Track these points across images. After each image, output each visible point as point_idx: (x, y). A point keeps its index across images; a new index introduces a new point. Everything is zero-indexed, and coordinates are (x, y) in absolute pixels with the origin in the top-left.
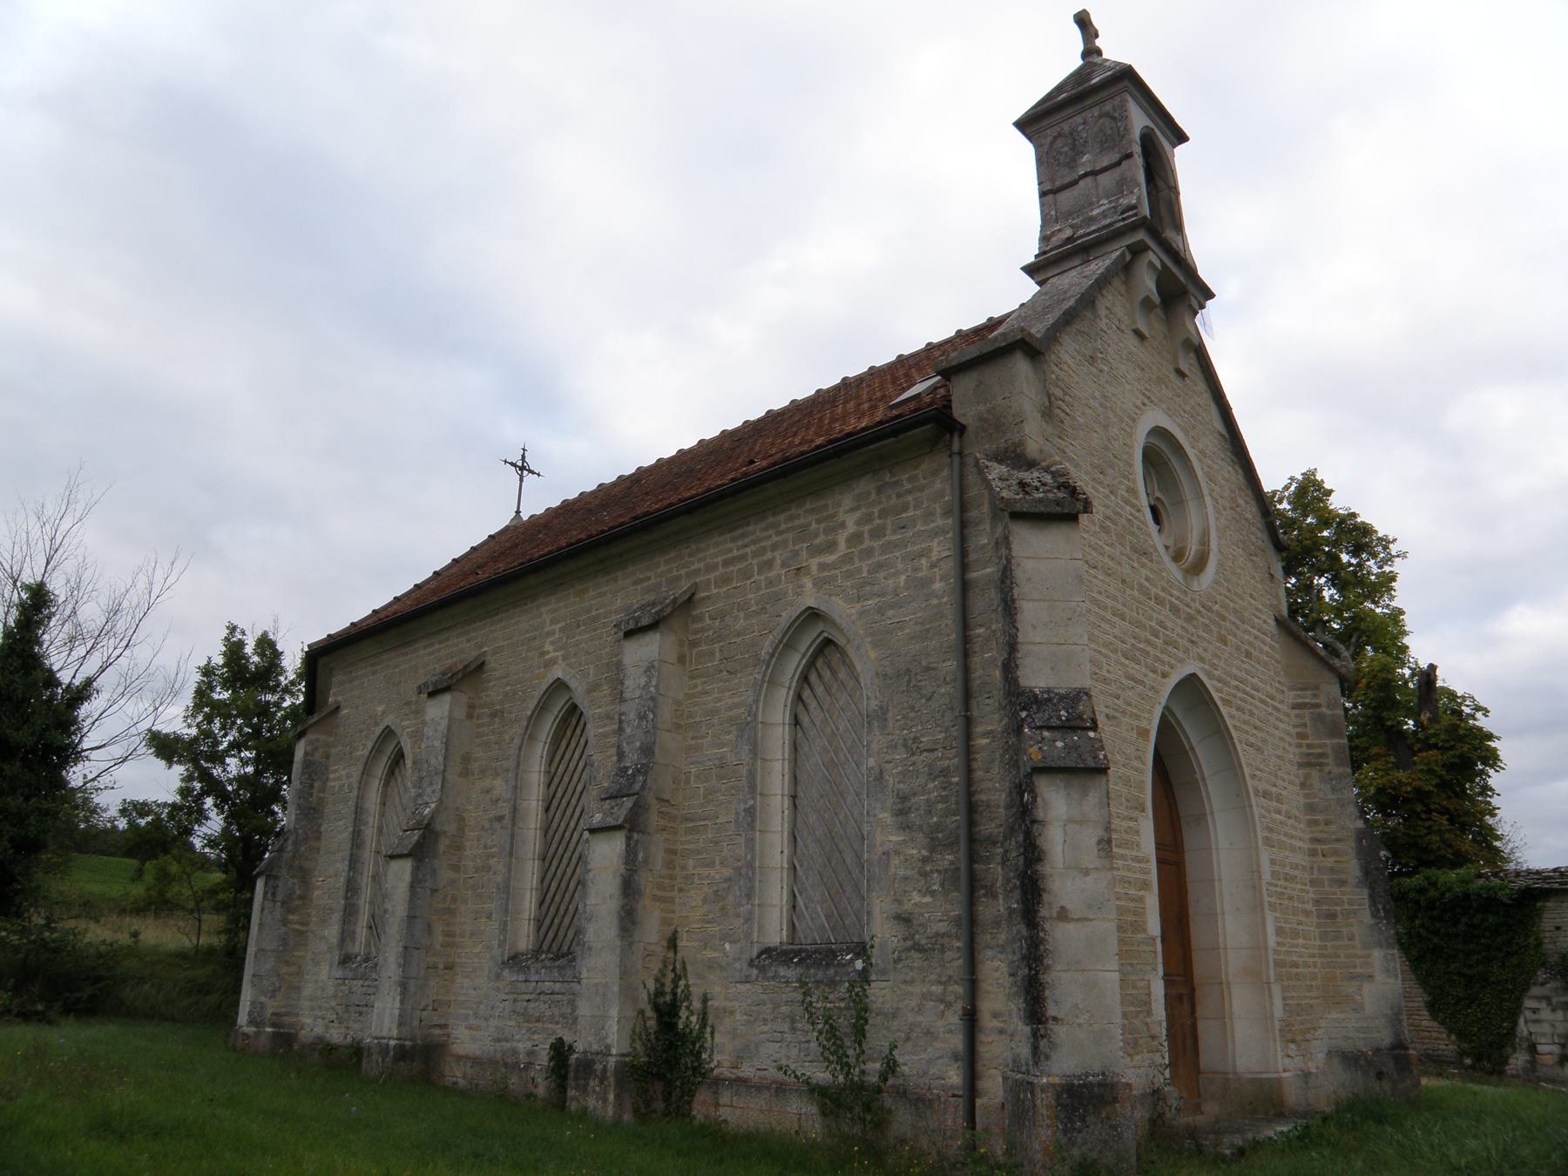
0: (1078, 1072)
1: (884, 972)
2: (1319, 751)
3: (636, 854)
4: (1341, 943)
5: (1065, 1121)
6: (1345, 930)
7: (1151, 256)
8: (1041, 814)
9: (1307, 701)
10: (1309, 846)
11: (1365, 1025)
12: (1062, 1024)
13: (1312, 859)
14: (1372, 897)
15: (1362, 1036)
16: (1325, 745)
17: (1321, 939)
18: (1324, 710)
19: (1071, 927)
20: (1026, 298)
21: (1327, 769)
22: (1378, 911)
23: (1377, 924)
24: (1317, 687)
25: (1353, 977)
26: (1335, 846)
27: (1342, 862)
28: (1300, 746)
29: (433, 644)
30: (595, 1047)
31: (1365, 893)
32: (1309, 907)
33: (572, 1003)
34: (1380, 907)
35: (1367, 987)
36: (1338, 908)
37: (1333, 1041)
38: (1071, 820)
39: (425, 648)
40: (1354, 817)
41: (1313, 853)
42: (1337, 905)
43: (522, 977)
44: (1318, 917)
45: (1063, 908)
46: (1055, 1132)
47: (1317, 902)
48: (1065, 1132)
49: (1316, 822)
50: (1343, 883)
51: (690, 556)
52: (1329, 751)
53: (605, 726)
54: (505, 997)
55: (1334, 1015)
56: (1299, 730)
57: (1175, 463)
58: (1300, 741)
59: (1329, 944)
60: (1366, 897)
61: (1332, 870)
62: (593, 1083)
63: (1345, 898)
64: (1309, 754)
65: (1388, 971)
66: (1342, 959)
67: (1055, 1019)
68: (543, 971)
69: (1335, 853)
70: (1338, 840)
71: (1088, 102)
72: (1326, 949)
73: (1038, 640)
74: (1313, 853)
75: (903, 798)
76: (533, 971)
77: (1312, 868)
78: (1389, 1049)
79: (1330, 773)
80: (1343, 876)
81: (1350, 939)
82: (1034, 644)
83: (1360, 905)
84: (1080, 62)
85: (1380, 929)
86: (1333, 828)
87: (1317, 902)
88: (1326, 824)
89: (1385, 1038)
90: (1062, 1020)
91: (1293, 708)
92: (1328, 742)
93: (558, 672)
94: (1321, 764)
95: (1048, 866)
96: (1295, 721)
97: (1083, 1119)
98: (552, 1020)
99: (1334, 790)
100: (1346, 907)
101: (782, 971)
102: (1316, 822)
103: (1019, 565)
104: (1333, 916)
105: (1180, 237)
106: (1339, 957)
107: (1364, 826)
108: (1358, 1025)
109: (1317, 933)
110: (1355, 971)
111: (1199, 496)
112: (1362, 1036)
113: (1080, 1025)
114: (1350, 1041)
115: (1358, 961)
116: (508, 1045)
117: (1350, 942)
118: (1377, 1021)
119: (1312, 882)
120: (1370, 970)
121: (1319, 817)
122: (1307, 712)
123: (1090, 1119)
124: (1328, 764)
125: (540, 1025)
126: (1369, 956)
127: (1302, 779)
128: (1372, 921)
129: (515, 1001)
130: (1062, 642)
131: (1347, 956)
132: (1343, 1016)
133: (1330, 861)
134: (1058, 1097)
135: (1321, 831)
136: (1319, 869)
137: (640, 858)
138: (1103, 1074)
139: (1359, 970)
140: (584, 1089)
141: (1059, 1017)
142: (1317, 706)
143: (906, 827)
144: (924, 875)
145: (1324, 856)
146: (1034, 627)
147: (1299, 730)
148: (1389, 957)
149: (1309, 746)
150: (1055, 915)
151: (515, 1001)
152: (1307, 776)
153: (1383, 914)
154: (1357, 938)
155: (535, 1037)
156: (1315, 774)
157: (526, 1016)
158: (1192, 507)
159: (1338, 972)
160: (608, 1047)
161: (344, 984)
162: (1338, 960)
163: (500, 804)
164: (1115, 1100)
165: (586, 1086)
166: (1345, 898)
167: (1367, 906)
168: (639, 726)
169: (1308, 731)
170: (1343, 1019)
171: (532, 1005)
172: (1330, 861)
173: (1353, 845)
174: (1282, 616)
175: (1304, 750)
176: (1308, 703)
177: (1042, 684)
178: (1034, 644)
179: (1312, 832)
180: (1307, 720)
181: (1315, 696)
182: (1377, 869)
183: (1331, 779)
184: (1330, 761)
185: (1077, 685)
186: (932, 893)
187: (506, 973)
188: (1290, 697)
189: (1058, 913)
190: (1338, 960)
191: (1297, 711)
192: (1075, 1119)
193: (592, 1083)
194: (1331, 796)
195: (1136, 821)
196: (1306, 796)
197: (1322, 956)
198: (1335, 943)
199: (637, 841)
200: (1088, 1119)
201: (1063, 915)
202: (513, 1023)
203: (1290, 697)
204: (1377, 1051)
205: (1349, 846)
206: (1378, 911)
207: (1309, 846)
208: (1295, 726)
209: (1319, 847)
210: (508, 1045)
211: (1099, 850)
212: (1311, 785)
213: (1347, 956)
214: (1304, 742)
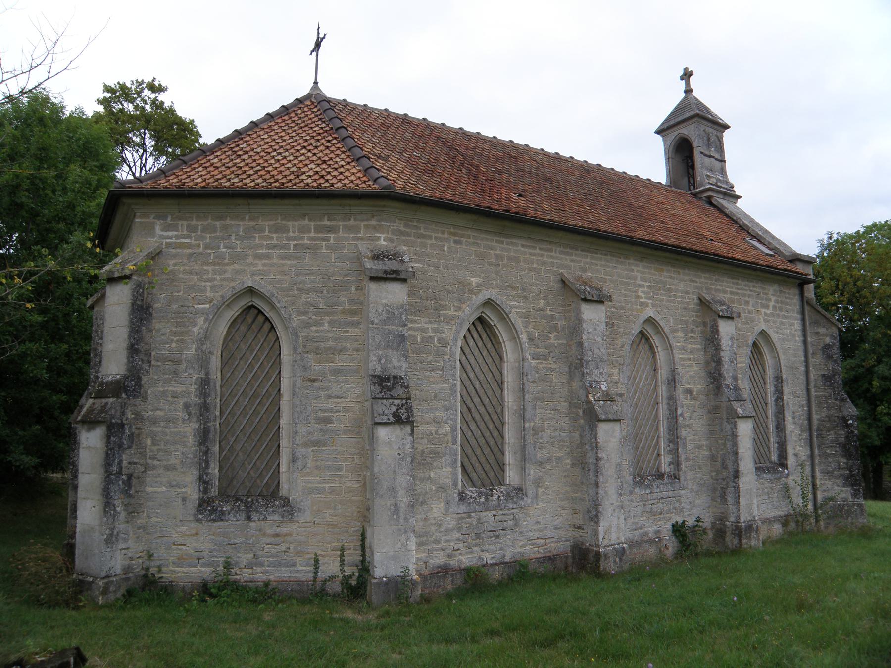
1: (792, 474)
20: (655, 179)
29: (535, 248)
30: (749, 518)
33: (679, 501)
39: (523, 246)
43: (648, 491)
51: (716, 281)
53: (683, 354)
54: (637, 504)
62: (753, 534)
68: (662, 486)
71: (715, 127)
75: (794, 413)
76: (655, 487)
84: (684, 95)
93: (650, 312)
98: (669, 512)
101: (765, 476)
116: (643, 531)
125: (662, 516)
129: (644, 505)
140: (750, 538)
143: (795, 423)
144: (800, 440)
151: (644, 505)
155: (659, 523)
157: (652, 513)
160: (754, 517)
161: (470, 517)
163: (619, 385)
165: (750, 537)
168: (730, 365)
171: (655, 506)
186: (802, 446)
187: (637, 490)
193: (753, 534)
202: (645, 518)
210: (643, 531)
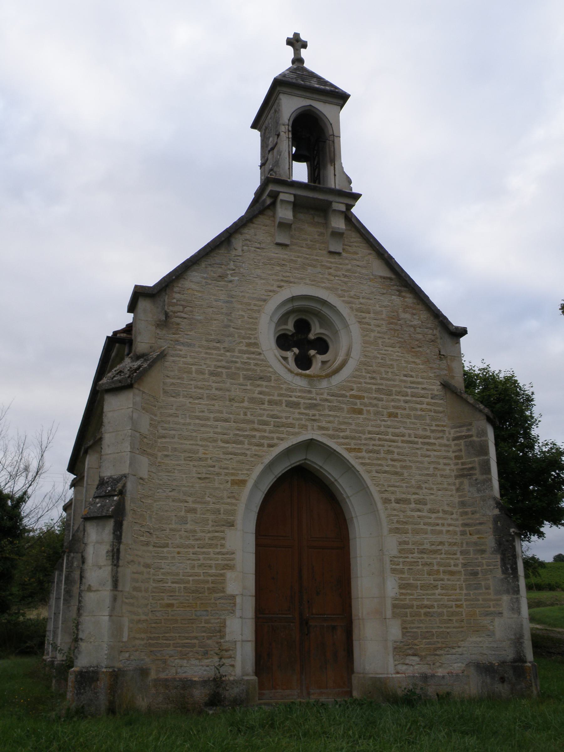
0: (88, 665)
2: (470, 466)
3: (72, 563)
4: (481, 591)
5: (78, 689)
6: (483, 583)
7: (282, 197)
8: (86, 540)
9: (463, 434)
10: (461, 529)
11: (495, 646)
12: (84, 642)
13: (463, 537)
14: (503, 560)
15: (493, 652)
16: (474, 461)
17: (467, 589)
18: (475, 438)
19: (92, 594)
21: (474, 477)
22: (507, 569)
23: (506, 578)
24: (470, 424)
25: (487, 614)
26: (479, 527)
27: (483, 538)
28: (457, 464)
31: (498, 557)
32: (459, 568)
34: (509, 566)
35: (498, 621)
36: (479, 568)
37: (473, 656)
38: (97, 542)
40: (492, 507)
41: (463, 533)
42: (479, 566)
44: (465, 575)
45: (89, 585)
46: (73, 694)
47: (464, 565)
48: (77, 694)
49: (466, 513)
50: (483, 551)
52: (477, 466)
55: (474, 639)
56: (457, 454)
57: (325, 311)
58: (457, 461)
59: (471, 592)
60: (499, 560)
61: (476, 544)
63: (484, 561)
64: (463, 469)
65: (513, 609)
66: (481, 602)
67: (81, 639)
69: (478, 532)
70: (481, 524)
72: (470, 596)
73: (109, 452)
74: (463, 533)
77: (462, 543)
78: (511, 662)
79: (476, 480)
80: (483, 547)
81: (487, 589)
82: (108, 454)
83: (495, 565)
85: (508, 581)
86: (477, 516)
87: (464, 565)
88: (473, 514)
89: (509, 654)
90: (84, 639)
91: (453, 440)
92: (476, 459)
94: (471, 475)
95: (86, 565)
96: (454, 448)
97: (84, 689)
99: (479, 491)
100: (485, 567)
102: (466, 513)
103: (106, 416)
104: (475, 574)
105: (332, 167)
106: (479, 600)
107: (499, 513)
108: (491, 645)
109: (464, 586)
110: (490, 609)
111: (346, 326)
112: (493, 652)
113: (91, 642)
114: (486, 656)
115: (492, 603)
117: (487, 591)
118: (505, 643)
119: (462, 553)
120: (501, 609)
121: (469, 510)
122: (462, 442)
123: (87, 688)
124: (475, 474)
126: (500, 600)
127: (458, 486)
128: (503, 576)
130: (119, 451)
131: (484, 600)
132: (480, 639)
133: (475, 538)
134: (76, 677)
135: (469, 518)
136: (467, 543)
137: (75, 565)
138: (97, 667)
139: (492, 609)
141: (83, 638)
142: (471, 436)
145: (470, 534)
146: (108, 446)
147: (457, 454)
148: (515, 600)
149: (463, 464)
150: (86, 589)
152: (461, 483)
153: (511, 572)
154: (491, 588)
156: (466, 481)
158: (343, 334)
159: (477, 610)
162: (478, 603)
164: (98, 680)
166: (484, 561)
167: (499, 567)
169: (463, 453)
170: (481, 642)
172: (475, 538)
173: (491, 526)
174: (453, 382)
175: (460, 466)
176: (464, 436)
177: (109, 474)
178: (108, 454)
179: (463, 520)
180: (463, 447)
181: (468, 430)
182: (507, 541)
183: (477, 484)
184: (477, 472)
185: (123, 473)
188: (453, 433)
189: (88, 588)
190: (478, 603)
191: (456, 442)
192: (82, 688)
194: (476, 495)
195: (224, 532)
196: (460, 496)
197: (466, 600)
198: (476, 591)
199: (73, 557)
200: (86, 688)
201: (89, 589)
203: (453, 433)
204: (503, 663)
205: (489, 527)
206: (507, 569)
207: (461, 529)
208: (453, 452)
209: (467, 529)
211: (107, 556)
212: (464, 489)
213: (484, 600)
214: (460, 461)
